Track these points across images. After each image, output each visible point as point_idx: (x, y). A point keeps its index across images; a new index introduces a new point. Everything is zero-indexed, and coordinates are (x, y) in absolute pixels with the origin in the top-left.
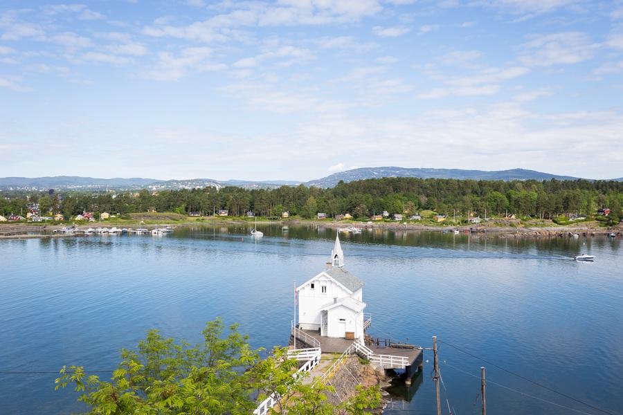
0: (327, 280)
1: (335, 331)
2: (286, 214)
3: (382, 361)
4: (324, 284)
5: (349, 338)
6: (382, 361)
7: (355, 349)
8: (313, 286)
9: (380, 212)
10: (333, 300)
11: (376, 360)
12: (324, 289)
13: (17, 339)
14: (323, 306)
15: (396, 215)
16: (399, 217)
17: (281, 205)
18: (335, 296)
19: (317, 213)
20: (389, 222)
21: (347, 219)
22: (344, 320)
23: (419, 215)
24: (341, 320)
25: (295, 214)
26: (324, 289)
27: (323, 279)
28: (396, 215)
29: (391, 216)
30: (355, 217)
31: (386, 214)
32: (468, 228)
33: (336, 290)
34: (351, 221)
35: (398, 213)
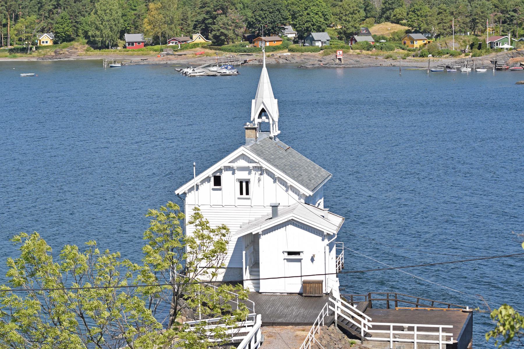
0: (251, 165)
1: (277, 277)
2: (46, 39)
3: (395, 336)
4: (244, 175)
5: (311, 293)
6: (419, 337)
7: (333, 313)
8: (218, 181)
9: (274, 30)
10: (270, 210)
11: (377, 335)
12: (244, 187)
13: (460, 306)
14: (250, 224)
15: (315, 35)
16: (320, 38)
17: (34, 17)
18: (274, 202)
19: (122, 33)
20: (298, 51)
21: (196, 45)
22: (298, 253)
23: (369, 34)
24: (290, 253)
25: (68, 39)
26: (244, 187)
27: (242, 163)
28: (315, 35)
29: (304, 36)
30: (218, 42)
31: (291, 33)
32: (486, 59)
33: (267, 191)
34: (207, 51)
35: (319, 29)
